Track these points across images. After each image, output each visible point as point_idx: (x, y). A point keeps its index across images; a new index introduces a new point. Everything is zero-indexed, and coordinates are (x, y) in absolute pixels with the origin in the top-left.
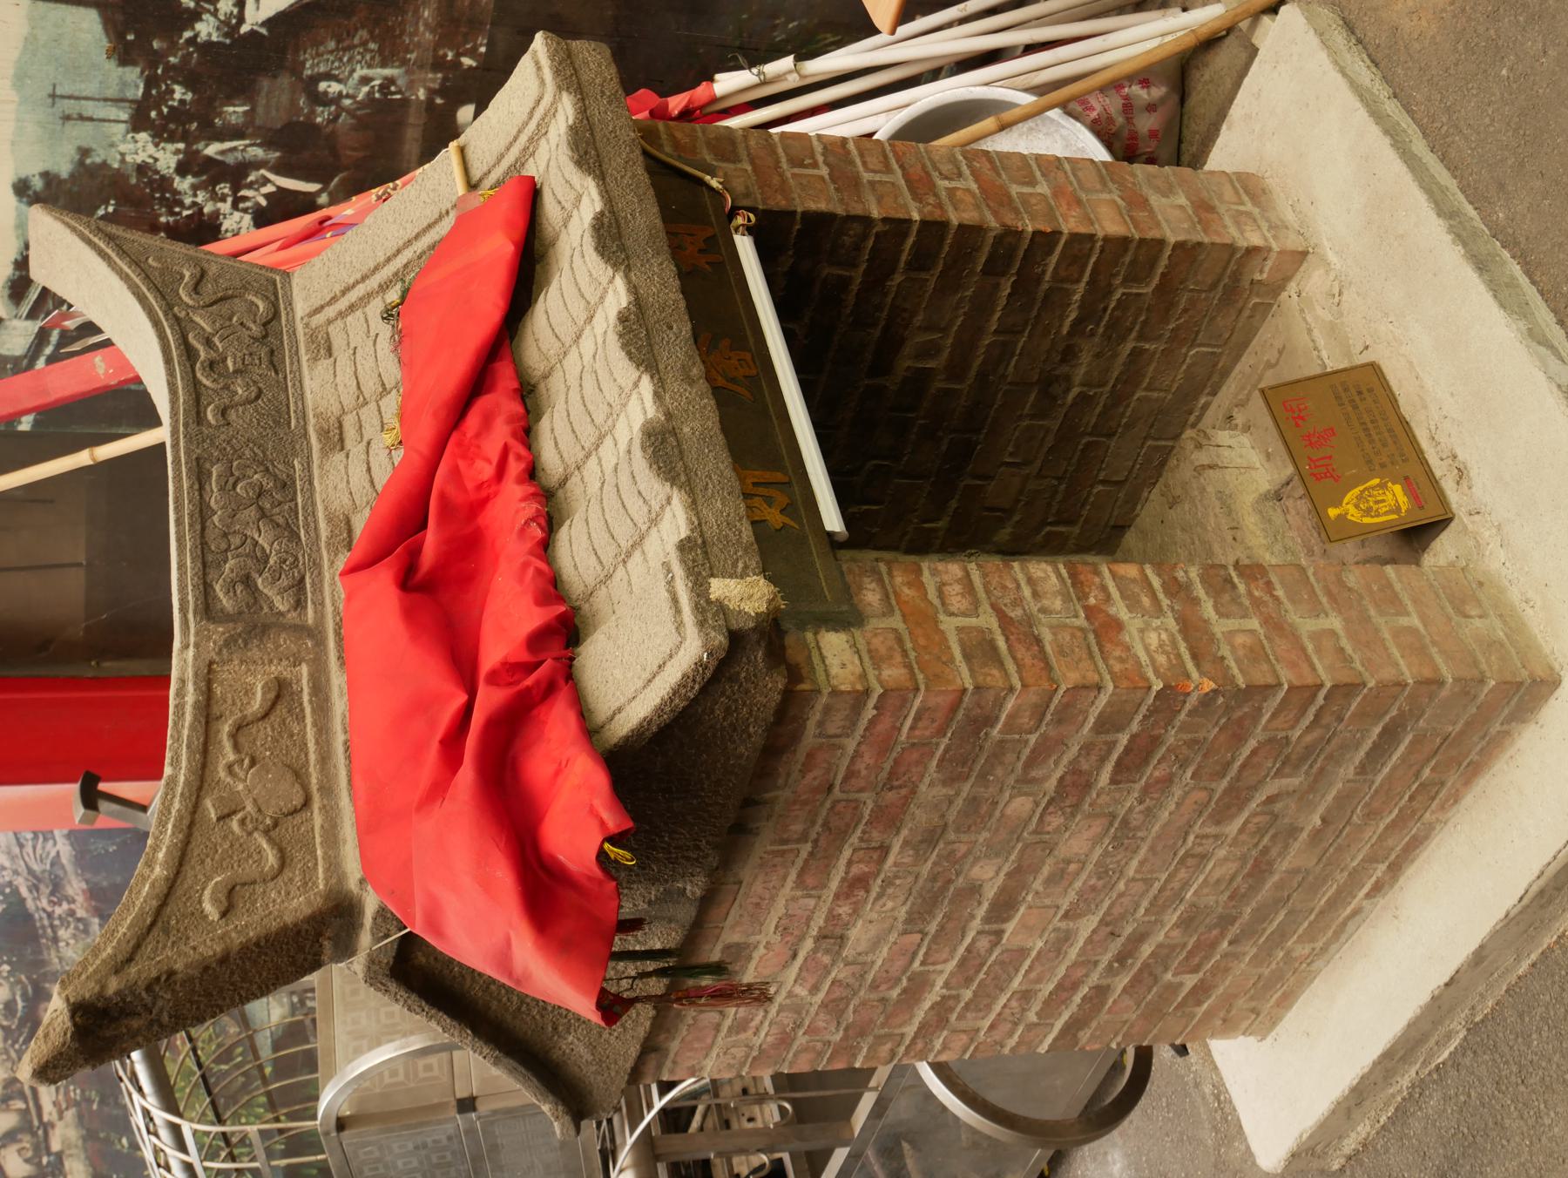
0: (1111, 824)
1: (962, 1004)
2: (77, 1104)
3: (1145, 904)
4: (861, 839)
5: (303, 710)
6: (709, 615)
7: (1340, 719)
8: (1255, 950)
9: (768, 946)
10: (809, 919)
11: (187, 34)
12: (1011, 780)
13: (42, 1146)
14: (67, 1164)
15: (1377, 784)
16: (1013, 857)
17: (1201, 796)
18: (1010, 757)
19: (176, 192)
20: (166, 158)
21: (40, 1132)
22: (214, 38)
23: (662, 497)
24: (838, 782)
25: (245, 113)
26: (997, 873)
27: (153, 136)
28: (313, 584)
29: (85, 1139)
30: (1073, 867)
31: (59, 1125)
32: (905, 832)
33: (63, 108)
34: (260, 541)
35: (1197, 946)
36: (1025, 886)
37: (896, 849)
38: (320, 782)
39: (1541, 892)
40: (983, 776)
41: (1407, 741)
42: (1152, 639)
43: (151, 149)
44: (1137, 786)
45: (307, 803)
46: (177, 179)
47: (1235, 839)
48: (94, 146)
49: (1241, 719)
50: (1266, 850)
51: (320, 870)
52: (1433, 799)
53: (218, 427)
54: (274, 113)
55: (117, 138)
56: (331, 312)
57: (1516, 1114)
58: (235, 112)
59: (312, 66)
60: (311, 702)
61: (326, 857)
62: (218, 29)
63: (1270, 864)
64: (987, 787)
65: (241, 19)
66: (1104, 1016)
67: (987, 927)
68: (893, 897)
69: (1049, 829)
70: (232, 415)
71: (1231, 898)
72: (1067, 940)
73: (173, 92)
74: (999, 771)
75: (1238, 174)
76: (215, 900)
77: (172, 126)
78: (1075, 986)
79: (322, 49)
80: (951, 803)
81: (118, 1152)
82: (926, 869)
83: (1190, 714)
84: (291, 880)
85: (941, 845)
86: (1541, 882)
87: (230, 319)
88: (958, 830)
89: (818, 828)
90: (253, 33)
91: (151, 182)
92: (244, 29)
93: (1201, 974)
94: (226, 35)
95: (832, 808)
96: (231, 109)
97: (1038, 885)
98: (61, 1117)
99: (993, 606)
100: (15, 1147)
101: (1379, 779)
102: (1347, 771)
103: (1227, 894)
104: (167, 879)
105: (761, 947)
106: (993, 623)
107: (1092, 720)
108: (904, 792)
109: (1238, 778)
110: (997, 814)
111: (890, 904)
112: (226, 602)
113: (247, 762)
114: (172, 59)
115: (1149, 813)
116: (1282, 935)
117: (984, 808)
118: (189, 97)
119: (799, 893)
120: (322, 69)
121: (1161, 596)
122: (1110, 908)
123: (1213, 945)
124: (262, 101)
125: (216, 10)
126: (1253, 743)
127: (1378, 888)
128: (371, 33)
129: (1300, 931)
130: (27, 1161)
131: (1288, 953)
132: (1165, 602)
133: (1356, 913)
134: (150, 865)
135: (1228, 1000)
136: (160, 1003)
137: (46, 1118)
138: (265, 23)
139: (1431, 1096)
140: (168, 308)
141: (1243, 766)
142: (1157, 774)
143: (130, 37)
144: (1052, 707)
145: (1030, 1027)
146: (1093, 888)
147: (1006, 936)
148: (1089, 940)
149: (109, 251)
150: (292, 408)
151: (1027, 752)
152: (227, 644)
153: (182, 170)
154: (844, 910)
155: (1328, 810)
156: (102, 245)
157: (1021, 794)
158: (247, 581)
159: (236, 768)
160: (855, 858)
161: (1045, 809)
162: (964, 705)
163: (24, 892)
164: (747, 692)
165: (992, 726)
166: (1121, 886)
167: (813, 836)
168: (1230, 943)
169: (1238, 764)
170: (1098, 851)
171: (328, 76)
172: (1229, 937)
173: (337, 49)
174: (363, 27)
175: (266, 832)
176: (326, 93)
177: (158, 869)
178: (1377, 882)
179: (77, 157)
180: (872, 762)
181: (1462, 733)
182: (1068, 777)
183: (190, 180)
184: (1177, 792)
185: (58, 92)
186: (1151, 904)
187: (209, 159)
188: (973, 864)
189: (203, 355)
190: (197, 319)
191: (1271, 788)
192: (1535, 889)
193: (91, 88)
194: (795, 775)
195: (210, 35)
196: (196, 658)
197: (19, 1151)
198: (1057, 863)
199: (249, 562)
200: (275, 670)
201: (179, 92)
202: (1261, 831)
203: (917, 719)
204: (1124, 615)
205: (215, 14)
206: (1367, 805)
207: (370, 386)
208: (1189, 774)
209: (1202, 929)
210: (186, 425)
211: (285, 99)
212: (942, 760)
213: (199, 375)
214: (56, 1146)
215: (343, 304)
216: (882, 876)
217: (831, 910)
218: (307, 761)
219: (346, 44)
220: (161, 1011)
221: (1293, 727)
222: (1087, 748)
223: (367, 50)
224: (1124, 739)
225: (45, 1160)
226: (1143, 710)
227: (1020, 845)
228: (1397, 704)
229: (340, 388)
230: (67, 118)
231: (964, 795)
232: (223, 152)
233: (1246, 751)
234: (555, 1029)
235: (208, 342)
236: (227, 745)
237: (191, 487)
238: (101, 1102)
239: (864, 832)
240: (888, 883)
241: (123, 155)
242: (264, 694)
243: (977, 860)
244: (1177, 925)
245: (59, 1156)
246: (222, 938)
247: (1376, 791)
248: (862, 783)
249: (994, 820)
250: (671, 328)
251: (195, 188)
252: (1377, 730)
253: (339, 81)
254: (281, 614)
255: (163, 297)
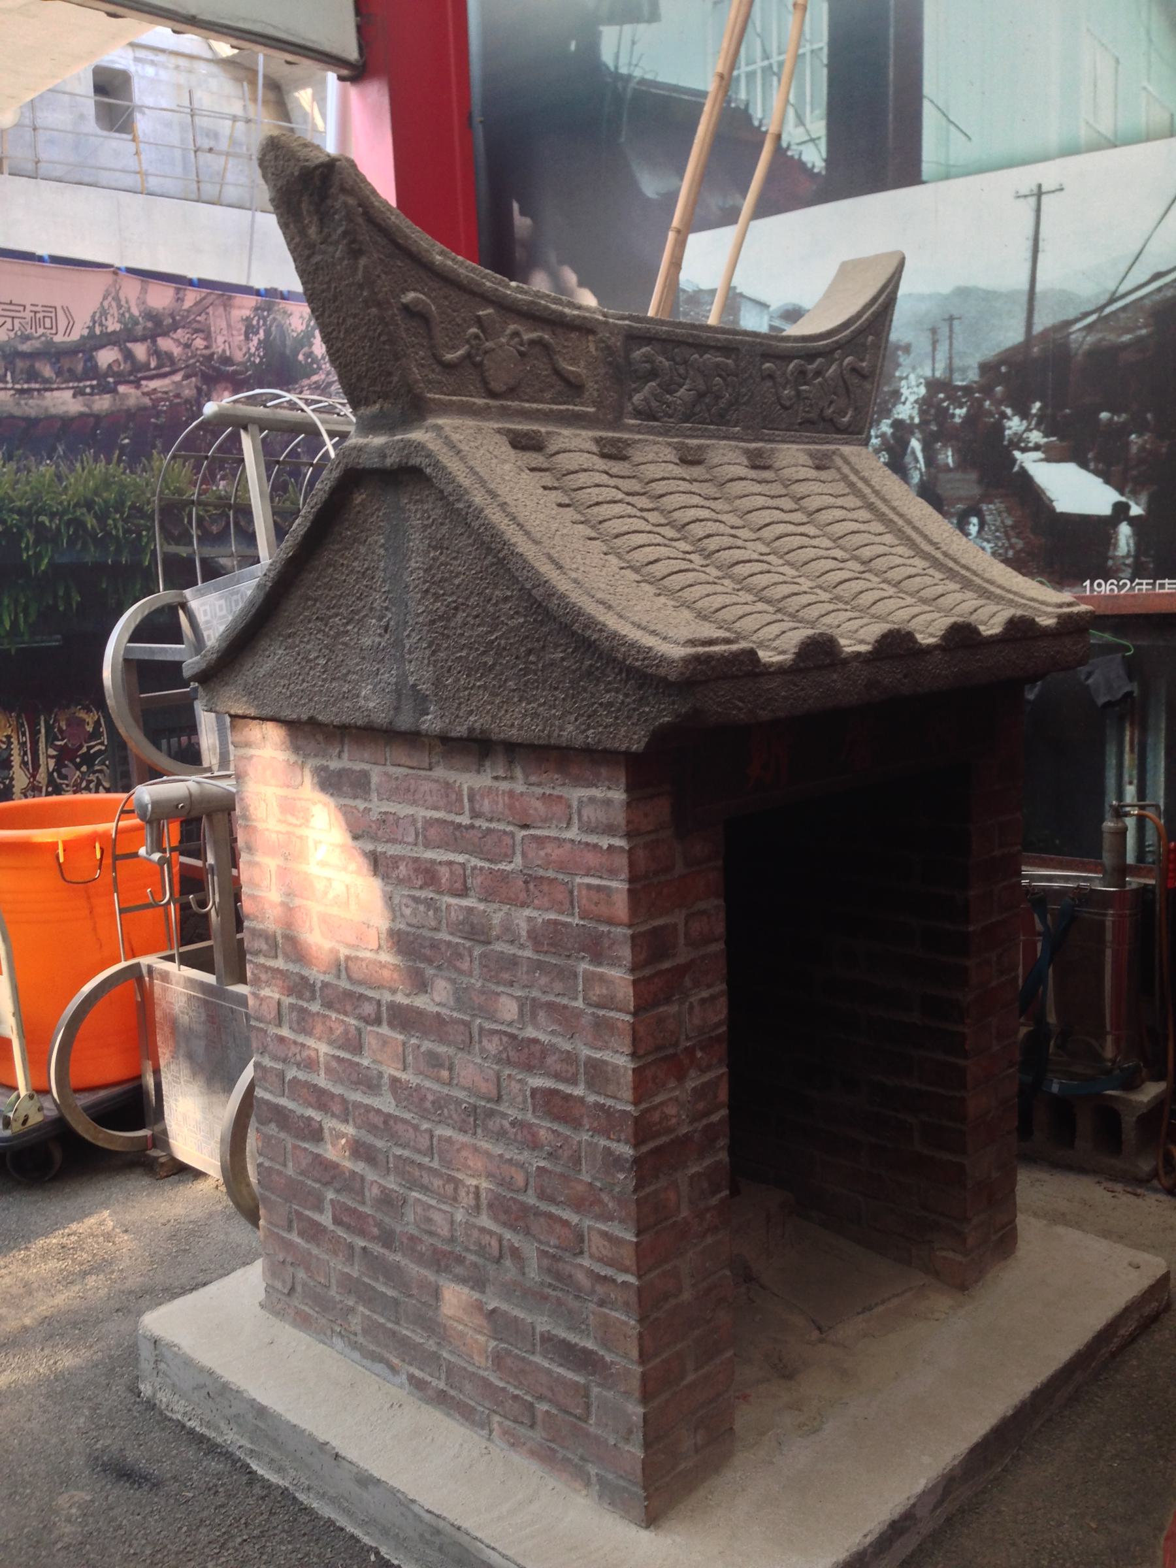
0: (489, 1100)
1: (305, 1005)
2: (155, 407)
3: (406, 1153)
4: (474, 868)
5: (560, 404)
6: (704, 667)
7: (602, 1303)
8: (355, 1275)
9: (367, 810)
10: (393, 841)
11: (1009, 411)
12: (535, 993)
13: (121, 379)
14: (107, 396)
15: (532, 1358)
16: (455, 1014)
17: (520, 1180)
18: (558, 986)
19: (878, 422)
20: (906, 411)
21: (132, 378)
22: (1007, 432)
23: (785, 647)
24: (532, 832)
25: (947, 464)
26: (438, 1004)
27: (923, 398)
28: (653, 427)
29: (128, 411)
30: (445, 1074)
31: (139, 393)
32: (482, 906)
33: (944, 324)
34: (682, 390)
35: (361, 1217)
36: (425, 1034)
37: (465, 902)
38: (509, 407)
39: (437, 1532)
40: (539, 966)
41: (577, 1378)
42: (671, 1110)
43: (912, 398)
44: (529, 1117)
45: (492, 395)
46: (889, 421)
47: (474, 1226)
48: (912, 355)
49: (600, 1201)
50: (460, 1260)
51: (442, 397)
52: (515, 1421)
53: (760, 369)
54: (949, 486)
55: (919, 371)
56: (846, 470)
57: (212, 1537)
58: (948, 457)
59: (989, 510)
60: (568, 410)
61: (452, 403)
62: (1015, 434)
63: (447, 1269)
64: (527, 973)
65: (1024, 450)
66: (290, 1142)
67: (384, 1009)
68: (415, 913)
69: (485, 1042)
70: (769, 384)
71: (412, 1238)
72: (369, 1087)
73: (961, 407)
74: (544, 980)
75: (1015, 1228)
76: (417, 301)
77: (933, 411)
78: (322, 1107)
79: (1005, 515)
80: (512, 942)
81: (118, 436)
82: (444, 936)
83: (607, 1149)
84: (433, 371)
85: (468, 944)
86: (449, 1528)
87: (835, 394)
88: (483, 955)
89: (485, 825)
90: (1014, 460)
91: (886, 402)
92: (1017, 454)
93: (332, 1227)
94: (1011, 441)
95: (505, 832)
96: (950, 453)
97: (427, 1045)
98: (144, 394)
99: (693, 961)
100: (120, 357)
101: (537, 1359)
102: (543, 1324)
103: (416, 1232)
104: (433, 263)
105: (366, 805)
106: (681, 959)
107: (598, 1055)
108: (522, 896)
109: (538, 1213)
110: (501, 989)
111: (408, 912)
112: (637, 354)
113: (522, 349)
114: (988, 403)
115: (501, 1135)
116: (369, 1297)
117: (506, 976)
118: (958, 420)
119: (419, 825)
120: (988, 518)
121: (705, 1122)
122: (405, 1121)
123: (362, 1233)
124: (958, 475)
125: (1031, 430)
126: (574, 1219)
127: (418, 1385)
128: (1021, 550)
129: (375, 1316)
130: (110, 366)
131: (352, 1310)
132: (700, 1125)
133: (394, 1370)
134: (441, 253)
135: (305, 1261)
136: (331, 249)
137: (143, 383)
138: (1022, 469)
139: (219, 1462)
140: (839, 346)
141: (550, 1216)
142: (542, 1132)
143: (1003, 369)
144: (612, 1014)
145: (281, 1075)
146: (423, 1099)
147: (375, 1029)
148: (368, 1109)
149: (876, 306)
150: (777, 432)
151: (565, 1001)
152: (608, 348)
153: (898, 424)
154: (403, 870)
155: (505, 1314)
156: (881, 300)
157: (521, 1008)
158: (653, 374)
159: (517, 340)
160: (456, 867)
161: (505, 1033)
162: (613, 929)
163: (315, 378)
164: (629, 717)
165: (591, 962)
166: (425, 1126)
167: (477, 823)
168: (364, 1249)
169: (553, 1209)
170: (461, 1095)
171: (982, 524)
172: (370, 1246)
173: (1005, 527)
174: (1026, 543)
175: (468, 356)
176: (969, 523)
177: (439, 257)
178: (426, 1383)
179: (902, 344)
180: (554, 857)
181: (587, 1435)
182: (538, 1047)
183: (889, 431)
184: (525, 1156)
185: (956, 322)
186: (407, 1158)
187: (908, 443)
188: (449, 979)
189: (810, 367)
190: (834, 367)
191: (530, 1250)
192: (441, 1524)
193: (958, 345)
194: (539, 791)
195: (1010, 428)
196: (597, 320)
197: (116, 361)
198: (449, 1057)
199: (667, 378)
200: (590, 385)
201: (961, 412)
202: (482, 1250)
203: (599, 888)
204: (690, 1084)
205: (1028, 430)
206: (508, 1353)
207: (800, 489)
208: (542, 1164)
209: (379, 1216)
210: (761, 344)
211: (962, 493)
212: (556, 922)
213: (796, 361)
214: (122, 389)
215: (853, 478)
216: (437, 897)
217: (402, 858)
218: (523, 401)
219: (1011, 533)
220: (324, 253)
221: (591, 1256)
222: (570, 1058)
223: (1007, 549)
224: (579, 1091)
225: (111, 380)
226: (609, 1102)
227: (467, 1018)
228: (618, 1359)
229: (794, 469)
230: (934, 331)
231: (520, 953)
232: (913, 452)
233: (567, 1215)
234: (289, 636)
235: (818, 373)
236: (534, 335)
237: (718, 340)
238: (156, 426)
239: (482, 868)
240: (429, 903)
241: (907, 378)
242: (573, 372)
243: (453, 981)
244: (383, 1189)
245: (114, 391)
246: (389, 303)
247: (523, 1359)
248: (531, 854)
249: (493, 987)
250: (905, 676)
251: (883, 436)
252: (590, 1345)
253: (979, 532)
254: (630, 398)
255: (849, 342)
